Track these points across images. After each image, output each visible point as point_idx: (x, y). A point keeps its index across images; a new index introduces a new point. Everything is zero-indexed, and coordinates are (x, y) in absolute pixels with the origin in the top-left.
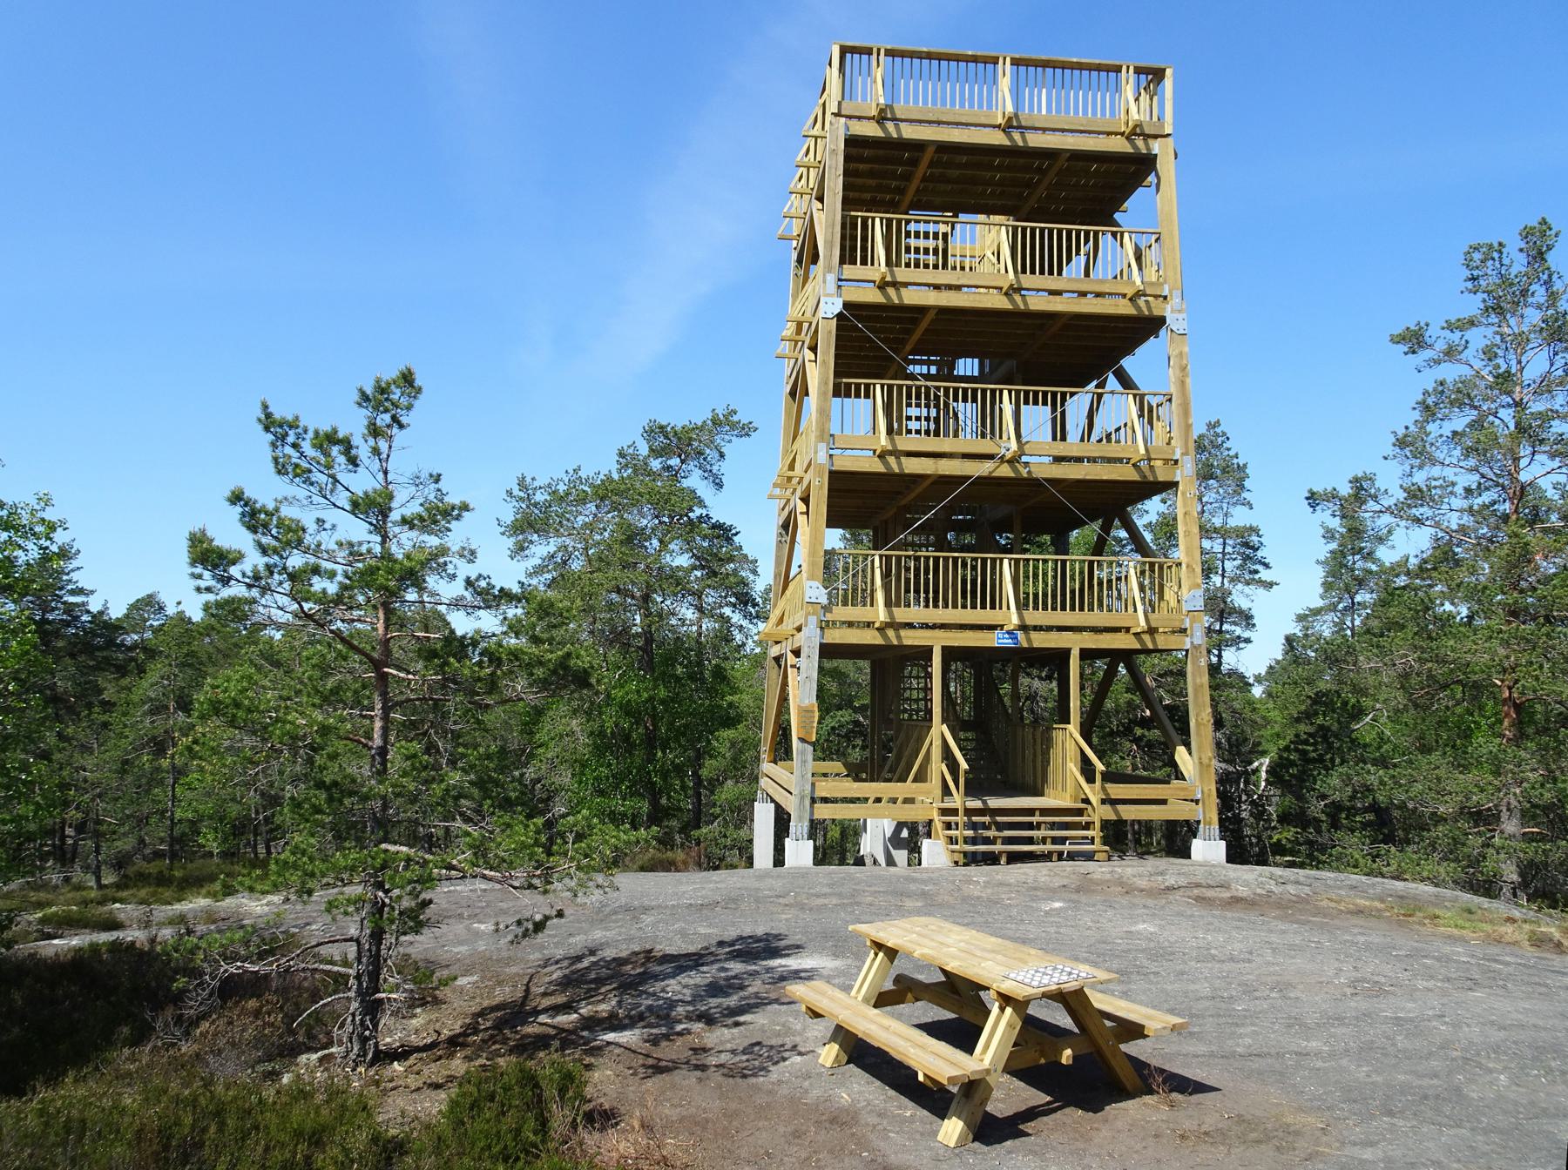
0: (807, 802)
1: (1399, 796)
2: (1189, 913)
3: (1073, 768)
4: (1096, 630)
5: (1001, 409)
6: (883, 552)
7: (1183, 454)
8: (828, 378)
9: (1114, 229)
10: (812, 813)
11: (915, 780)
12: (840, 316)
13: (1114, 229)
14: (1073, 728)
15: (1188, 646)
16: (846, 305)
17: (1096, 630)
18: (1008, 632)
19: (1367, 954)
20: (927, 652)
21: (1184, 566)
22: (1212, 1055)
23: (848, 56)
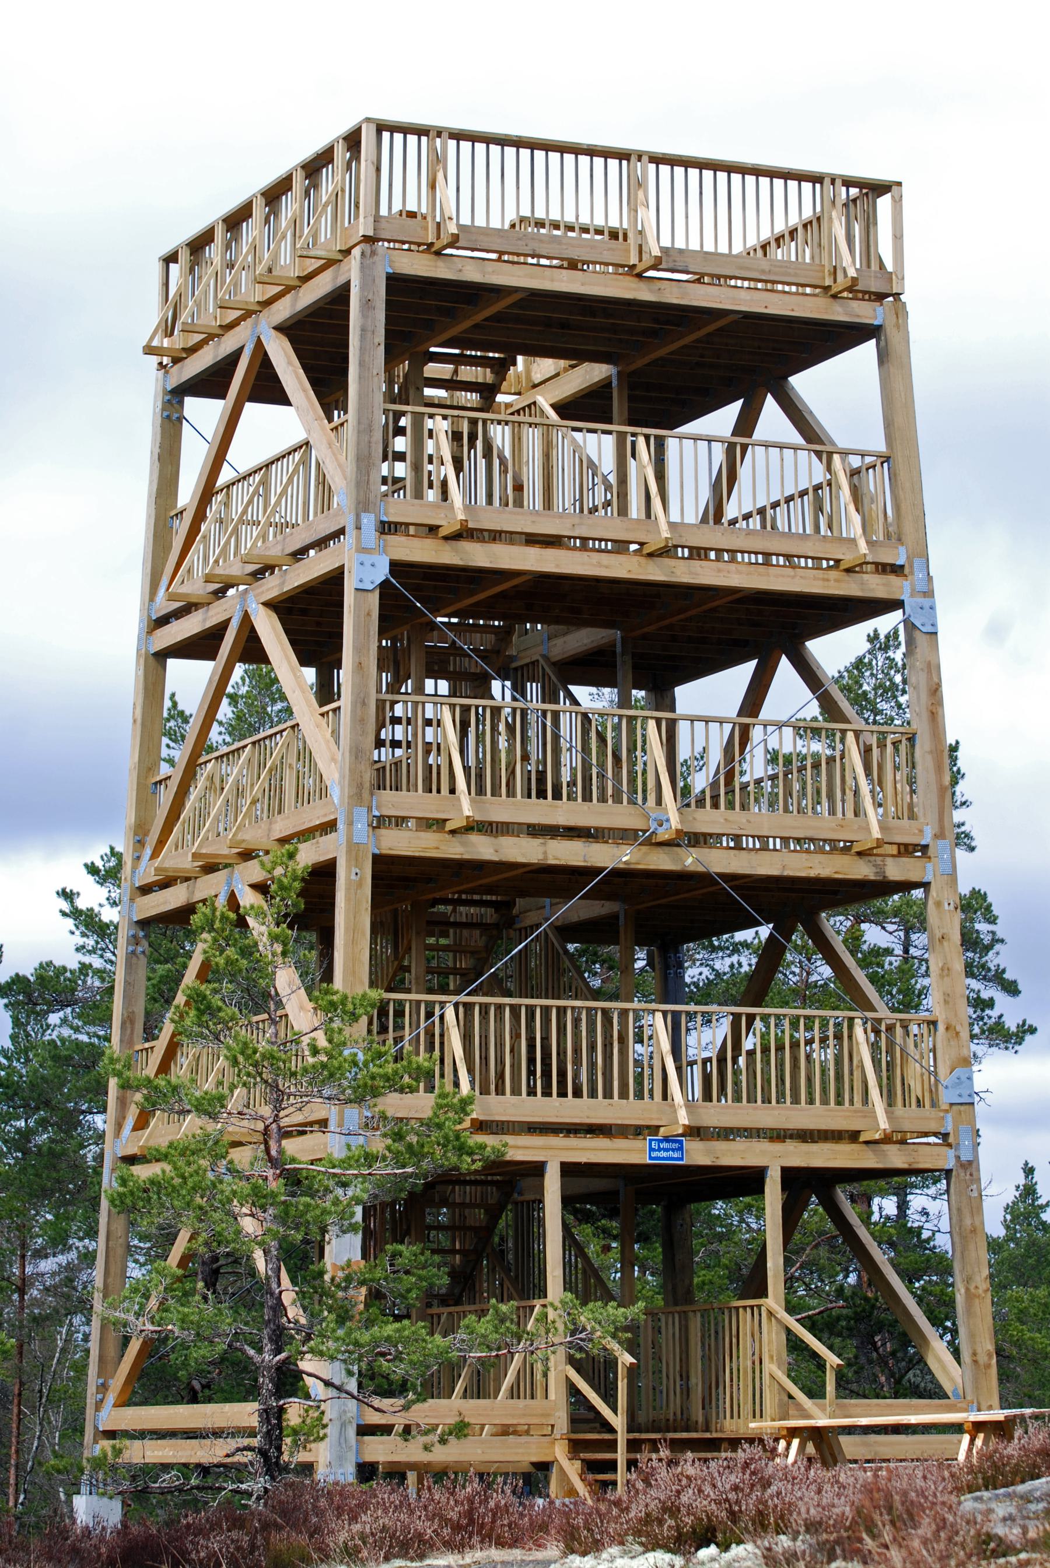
0: (352, 1431)
1: (456, 1557)
2: (942, 1534)
3: (775, 1370)
4: (806, 1136)
5: (644, 736)
6: (463, 998)
7: (936, 836)
8: (367, 695)
9: (818, 447)
10: (358, 1452)
11: (514, 1393)
12: (384, 585)
13: (818, 447)
14: (774, 1300)
15: (950, 1164)
16: (397, 567)
17: (806, 1136)
18: (666, 1139)
19: (148, 950)
20: (537, 1169)
21: (941, 1027)
22: (926, 1460)
23: (386, 135)
